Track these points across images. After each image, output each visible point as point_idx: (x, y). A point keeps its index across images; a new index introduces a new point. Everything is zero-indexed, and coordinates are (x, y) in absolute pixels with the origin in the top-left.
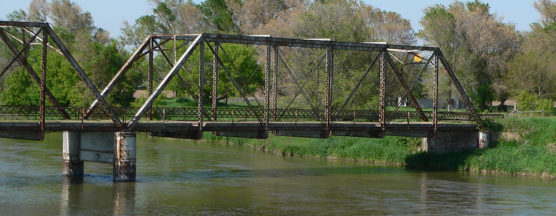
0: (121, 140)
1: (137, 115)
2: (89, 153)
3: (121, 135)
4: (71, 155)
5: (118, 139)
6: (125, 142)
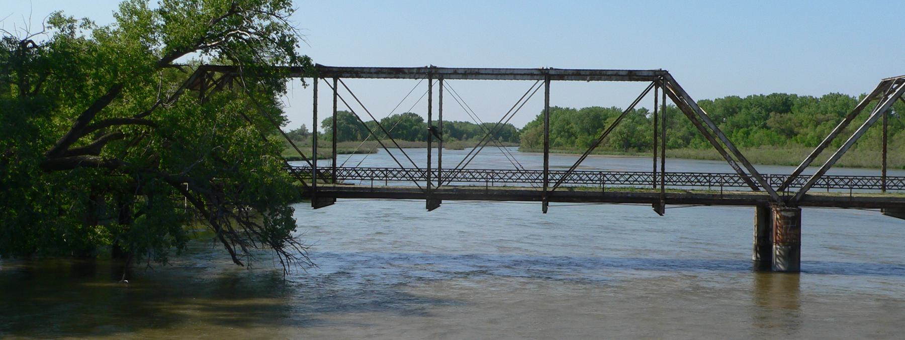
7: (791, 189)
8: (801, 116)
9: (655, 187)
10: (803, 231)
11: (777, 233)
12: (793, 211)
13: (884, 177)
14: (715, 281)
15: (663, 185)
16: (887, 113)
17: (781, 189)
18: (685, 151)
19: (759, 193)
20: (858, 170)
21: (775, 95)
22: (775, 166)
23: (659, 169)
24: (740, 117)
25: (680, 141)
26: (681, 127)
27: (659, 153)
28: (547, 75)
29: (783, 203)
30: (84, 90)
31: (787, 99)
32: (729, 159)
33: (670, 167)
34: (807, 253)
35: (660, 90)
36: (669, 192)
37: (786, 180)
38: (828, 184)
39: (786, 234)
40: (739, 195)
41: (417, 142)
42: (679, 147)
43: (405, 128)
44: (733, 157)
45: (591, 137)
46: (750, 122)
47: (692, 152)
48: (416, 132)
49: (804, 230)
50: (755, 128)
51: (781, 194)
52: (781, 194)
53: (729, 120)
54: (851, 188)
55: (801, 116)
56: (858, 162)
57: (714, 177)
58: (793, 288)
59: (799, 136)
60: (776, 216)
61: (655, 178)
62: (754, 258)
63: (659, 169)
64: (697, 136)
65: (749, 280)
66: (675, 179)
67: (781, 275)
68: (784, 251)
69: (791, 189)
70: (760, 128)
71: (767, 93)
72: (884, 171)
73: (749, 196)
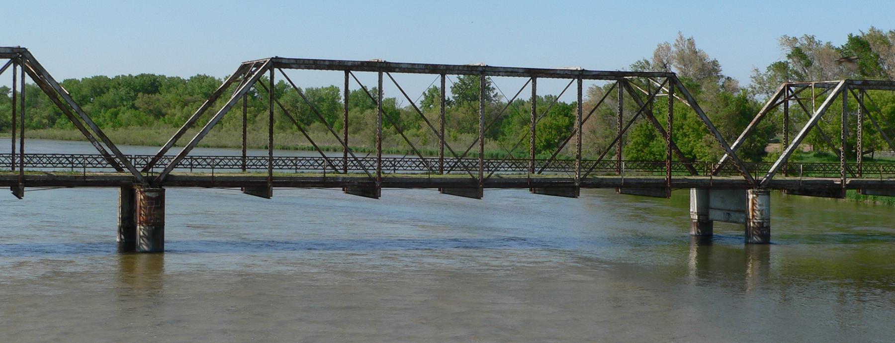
0: (753, 198)
1: (771, 171)
2: (718, 212)
3: (753, 193)
4: (698, 214)
5: (751, 197)
6: (758, 201)
7: (155, 170)
8: (169, 97)
9: (13, 169)
10: (167, 211)
11: (140, 214)
12: (157, 191)
13: (244, 156)
14: (82, 263)
15: (22, 167)
16: (246, 94)
17: (145, 170)
18: (50, 131)
19: (122, 174)
20: (219, 150)
21: (142, 75)
22: (139, 148)
23: (17, 151)
24: (107, 98)
25: (45, 121)
26: (46, 108)
27: (18, 134)
28: (534, 74)
29: (147, 184)
31: (154, 80)
32: (92, 140)
33: (31, 148)
34: (172, 231)
35: (19, 68)
36: (29, 174)
37: (150, 160)
38: (191, 164)
39: (150, 215)
40: (102, 177)
42: (44, 127)
44: (96, 137)
46: (118, 103)
47: (57, 132)
49: (167, 210)
50: (123, 109)
51: (145, 174)
52: (145, 174)
53: (97, 100)
54: (213, 168)
55: (169, 97)
56: (223, 142)
57: (77, 158)
58: (158, 267)
59: (166, 117)
60: (140, 197)
61: (13, 160)
62: (118, 240)
63: (17, 151)
64: (63, 116)
65: (111, 261)
66: (35, 160)
67: (145, 256)
68: (147, 231)
69: (155, 170)
70: (128, 109)
72: (244, 151)
73: (113, 177)
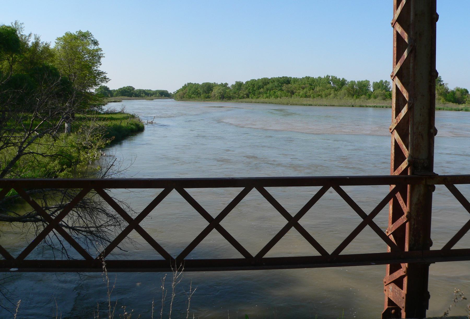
8: (295, 85)
24: (269, 86)
25: (245, 96)
30: (225, 95)
41: (133, 98)
43: (128, 92)
45: (207, 95)
48: (133, 93)
55: (295, 85)
71: (281, 76)
